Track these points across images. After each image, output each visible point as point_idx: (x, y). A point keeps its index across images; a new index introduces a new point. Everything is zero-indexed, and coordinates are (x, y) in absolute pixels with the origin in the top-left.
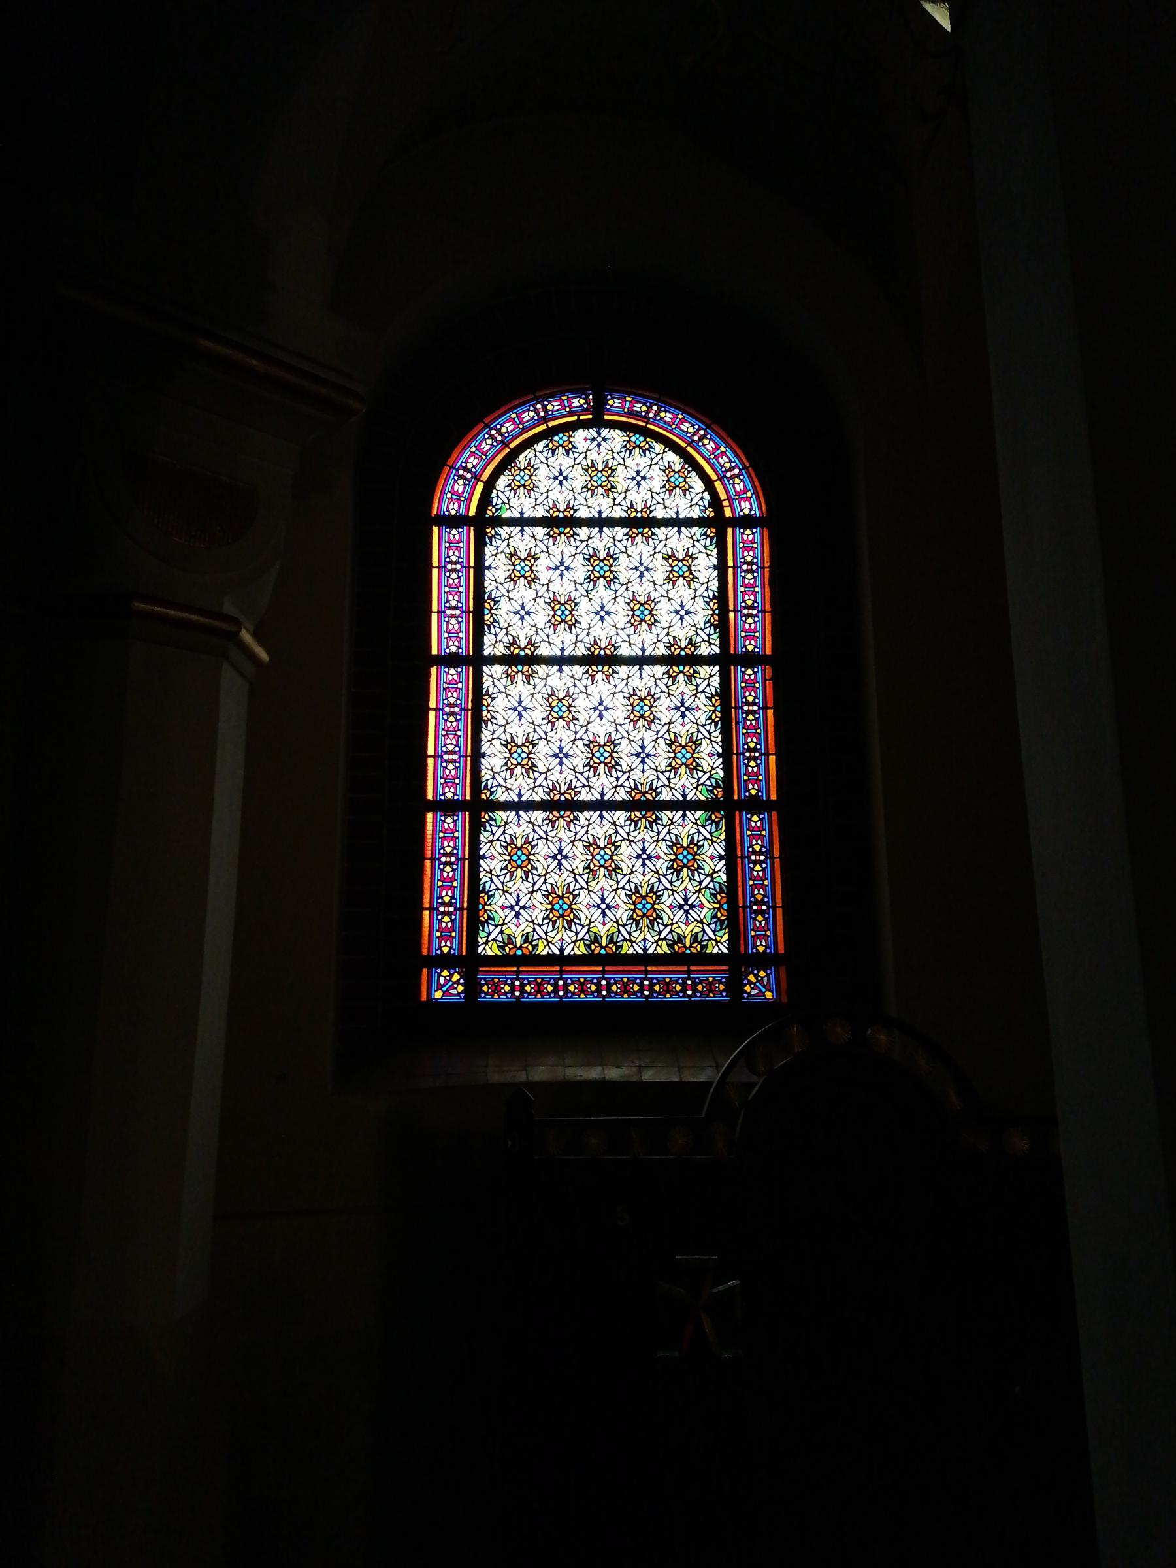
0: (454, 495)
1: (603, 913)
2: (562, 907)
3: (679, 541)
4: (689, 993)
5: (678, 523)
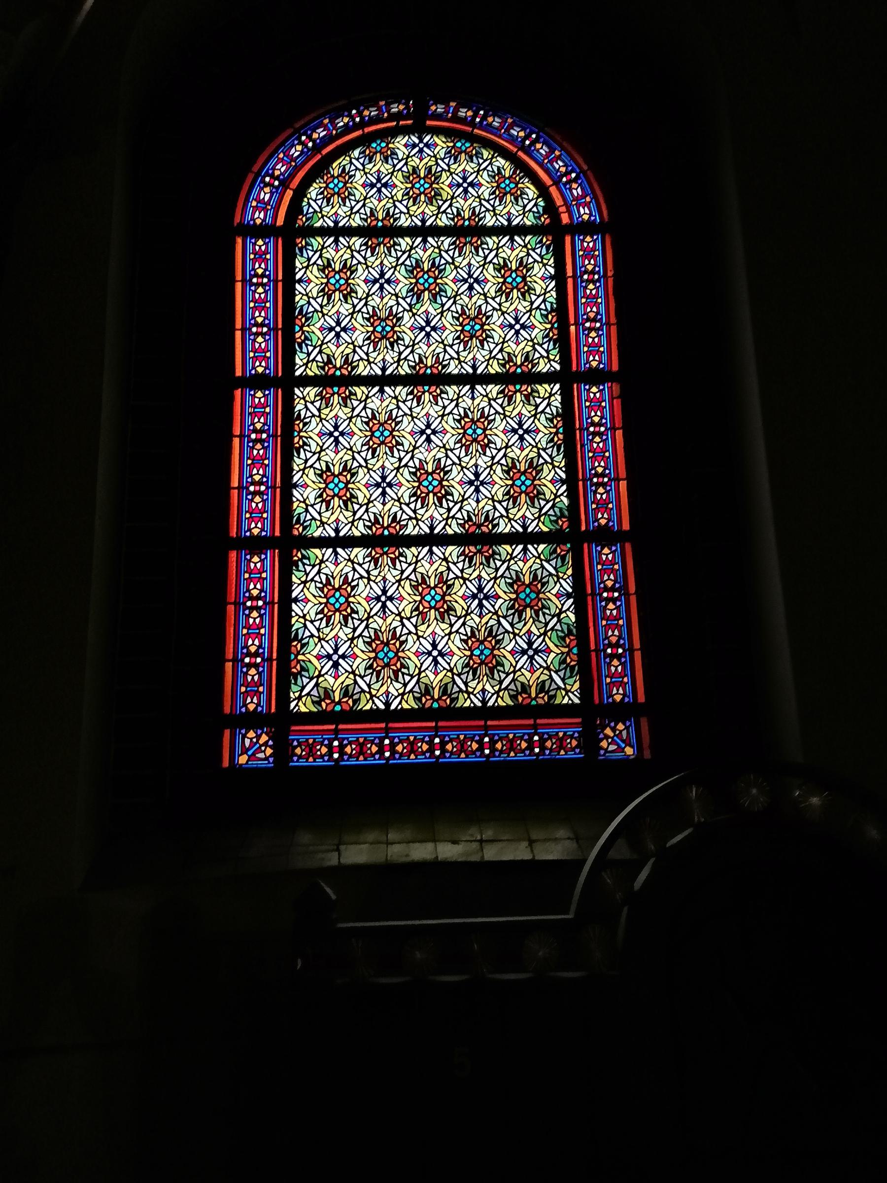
0: (261, 204)
2: (386, 654)
3: (512, 252)
5: (511, 231)
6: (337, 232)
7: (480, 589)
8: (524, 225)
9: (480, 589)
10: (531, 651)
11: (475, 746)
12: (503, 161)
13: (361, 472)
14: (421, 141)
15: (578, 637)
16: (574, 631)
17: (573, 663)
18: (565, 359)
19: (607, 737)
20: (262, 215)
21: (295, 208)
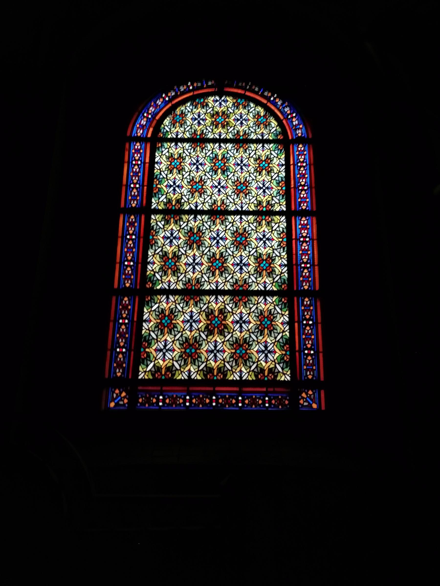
0: (140, 127)
1: (217, 353)
3: (263, 152)
4: (267, 405)
5: (263, 141)
6: (176, 140)
7: (241, 318)
8: (269, 139)
9: (241, 318)
10: (266, 352)
11: (234, 401)
12: (260, 108)
13: (183, 257)
14: (220, 98)
15: (287, 234)
16: (286, 282)
17: (284, 246)
18: (288, 205)
19: (303, 398)
20: (141, 131)
21: (157, 129)
